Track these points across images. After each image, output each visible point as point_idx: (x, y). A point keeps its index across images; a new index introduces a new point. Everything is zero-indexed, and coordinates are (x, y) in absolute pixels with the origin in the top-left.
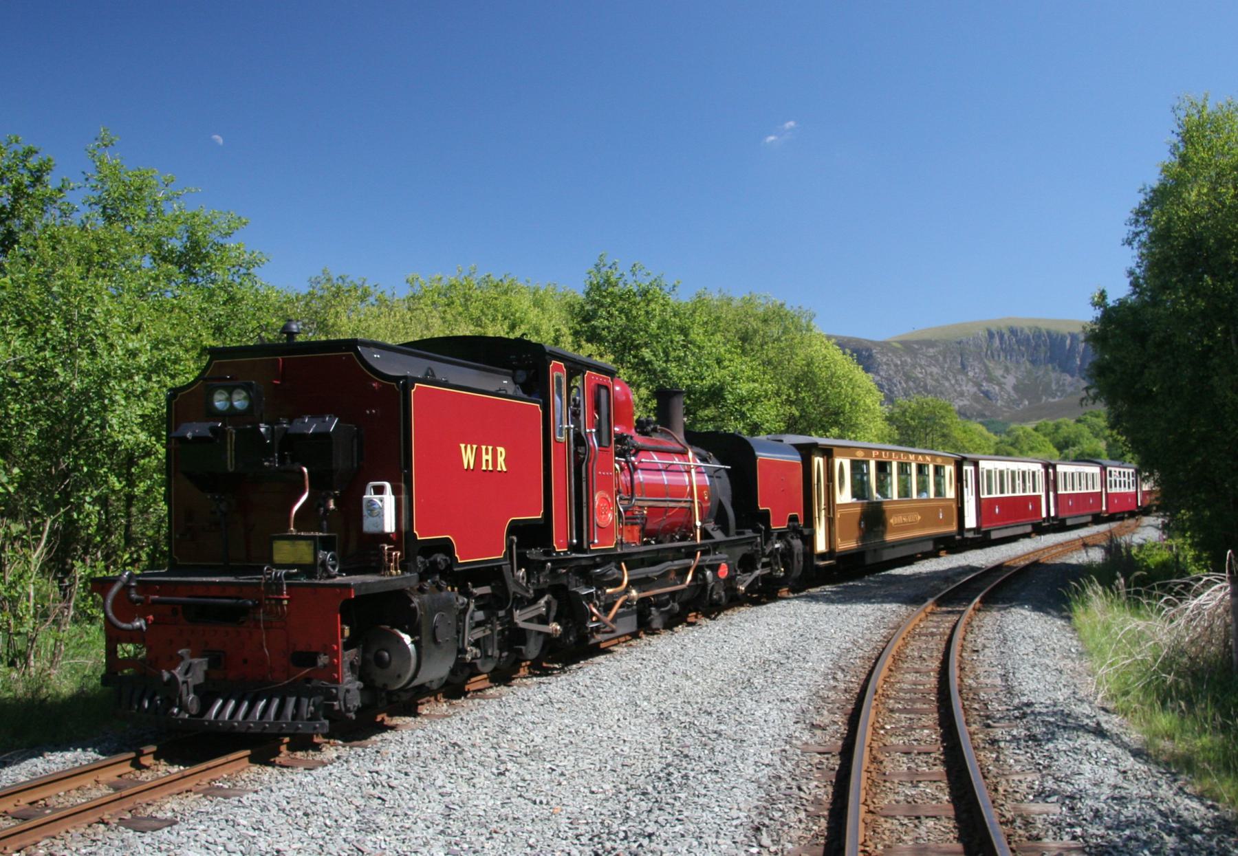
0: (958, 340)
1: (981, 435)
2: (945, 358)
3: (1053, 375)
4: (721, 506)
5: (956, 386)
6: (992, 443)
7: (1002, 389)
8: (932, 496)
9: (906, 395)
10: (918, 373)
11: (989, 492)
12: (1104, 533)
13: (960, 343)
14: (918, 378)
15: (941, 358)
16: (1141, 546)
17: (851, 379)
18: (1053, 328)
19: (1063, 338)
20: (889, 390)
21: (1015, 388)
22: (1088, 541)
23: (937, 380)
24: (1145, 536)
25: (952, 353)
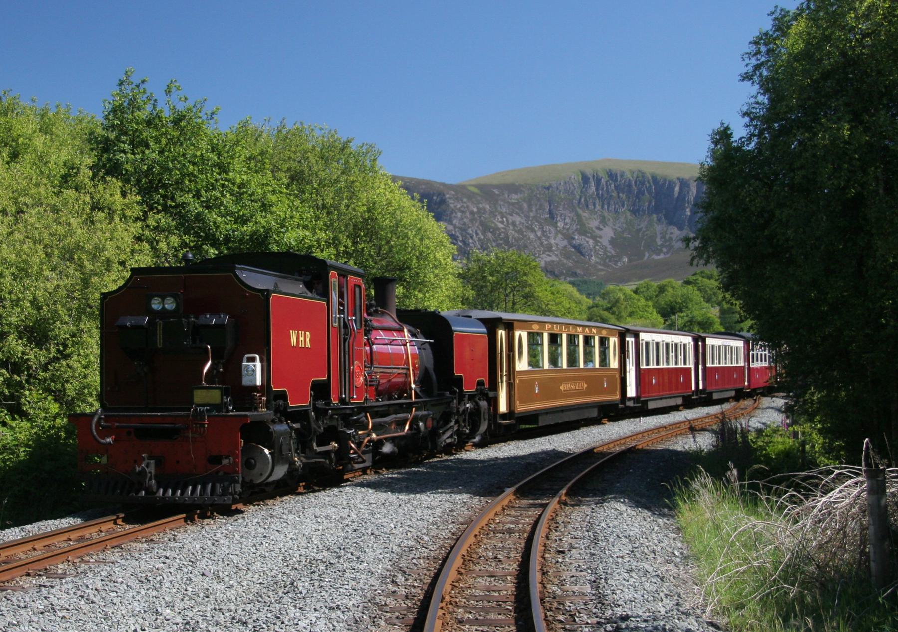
0: (547, 184)
1: (570, 297)
2: (530, 206)
3: (658, 228)
6: (584, 307)
7: (596, 242)
8: (597, 366)
9: (484, 248)
11: (647, 364)
12: (716, 416)
13: (548, 188)
14: (498, 229)
15: (525, 205)
16: (759, 432)
17: (420, 229)
18: (660, 172)
20: (464, 242)
21: (612, 242)
22: (697, 424)
23: (520, 232)
24: (764, 420)
25: (539, 200)
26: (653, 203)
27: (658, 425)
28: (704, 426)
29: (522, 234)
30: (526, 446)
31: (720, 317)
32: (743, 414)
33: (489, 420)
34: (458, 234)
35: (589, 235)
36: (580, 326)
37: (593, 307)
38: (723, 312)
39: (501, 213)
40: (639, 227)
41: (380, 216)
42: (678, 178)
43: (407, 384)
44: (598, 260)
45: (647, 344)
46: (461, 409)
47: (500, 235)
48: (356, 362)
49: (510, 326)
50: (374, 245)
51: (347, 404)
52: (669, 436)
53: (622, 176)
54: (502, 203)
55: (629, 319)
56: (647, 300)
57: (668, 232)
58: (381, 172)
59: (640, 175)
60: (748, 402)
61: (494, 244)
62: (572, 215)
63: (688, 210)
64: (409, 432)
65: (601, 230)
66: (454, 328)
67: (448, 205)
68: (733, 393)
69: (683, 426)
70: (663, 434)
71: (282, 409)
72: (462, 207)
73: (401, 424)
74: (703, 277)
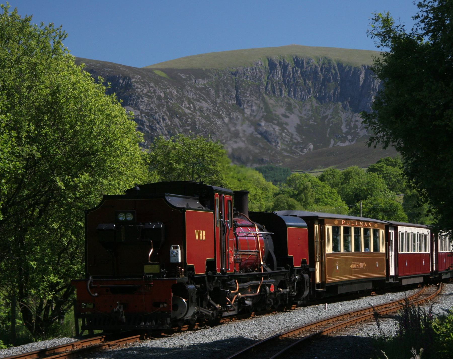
0: (234, 70)
1: (257, 183)
2: (217, 92)
3: (343, 116)
4: (269, 253)
5: (230, 125)
6: (270, 194)
7: (283, 129)
8: (372, 251)
9: (171, 134)
10: (185, 108)
11: (402, 251)
12: (399, 302)
13: (235, 74)
14: (185, 114)
15: (213, 91)
16: (442, 318)
17: (108, 115)
18: (345, 59)
19: (357, 72)
20: (151, 127)
21: (299, 129)
22: (380, 310)
23: (207, 118)
24: (446, 307)
25: (226, 86)
26: (339, 91)
27: (343, 311)
28: (388, 312)
29: (209, 120)
30: (212, 334)
31: (403, 205)
32: (426, 301)
33: (310, 288)
34: (144, 119)
35: (276, 122)
36: (362, 221)
37: (279, 194)
38: (407, 199)
39: (188, 99)
40: (325, 115)
41: (64, 100)
42: (364, 66)
43: (258, 261)
44: (284, 147)
45: (402, 234)
46: (293, 279)
47: (187, 120)
48: (229, 248)
49: (322, 222)
50: (58, 129)
51: (225, 273)
52: (354, 323)
53: (308, 63)
54: (189, 88)
55: (315, 206)
56: (332, 187)
57: (354, 119)
58: (66, 54)
59: (326, 61)
60: (431, 289)
61: (181, 130)
62: (258, 102)
63: (373, 97)
64: (260, 294)
65: (287, 117)
66: (287, 223)
67: (134, 90)
68: (421, 280)
69: (367, 312)
70: (348, 320)
71: (191, 276)
72: (148, 92)
73: (254, 288)
74: (388, 165)
